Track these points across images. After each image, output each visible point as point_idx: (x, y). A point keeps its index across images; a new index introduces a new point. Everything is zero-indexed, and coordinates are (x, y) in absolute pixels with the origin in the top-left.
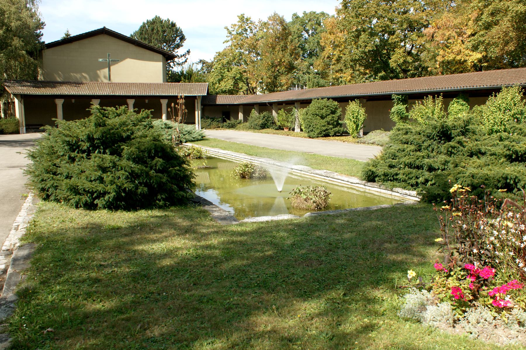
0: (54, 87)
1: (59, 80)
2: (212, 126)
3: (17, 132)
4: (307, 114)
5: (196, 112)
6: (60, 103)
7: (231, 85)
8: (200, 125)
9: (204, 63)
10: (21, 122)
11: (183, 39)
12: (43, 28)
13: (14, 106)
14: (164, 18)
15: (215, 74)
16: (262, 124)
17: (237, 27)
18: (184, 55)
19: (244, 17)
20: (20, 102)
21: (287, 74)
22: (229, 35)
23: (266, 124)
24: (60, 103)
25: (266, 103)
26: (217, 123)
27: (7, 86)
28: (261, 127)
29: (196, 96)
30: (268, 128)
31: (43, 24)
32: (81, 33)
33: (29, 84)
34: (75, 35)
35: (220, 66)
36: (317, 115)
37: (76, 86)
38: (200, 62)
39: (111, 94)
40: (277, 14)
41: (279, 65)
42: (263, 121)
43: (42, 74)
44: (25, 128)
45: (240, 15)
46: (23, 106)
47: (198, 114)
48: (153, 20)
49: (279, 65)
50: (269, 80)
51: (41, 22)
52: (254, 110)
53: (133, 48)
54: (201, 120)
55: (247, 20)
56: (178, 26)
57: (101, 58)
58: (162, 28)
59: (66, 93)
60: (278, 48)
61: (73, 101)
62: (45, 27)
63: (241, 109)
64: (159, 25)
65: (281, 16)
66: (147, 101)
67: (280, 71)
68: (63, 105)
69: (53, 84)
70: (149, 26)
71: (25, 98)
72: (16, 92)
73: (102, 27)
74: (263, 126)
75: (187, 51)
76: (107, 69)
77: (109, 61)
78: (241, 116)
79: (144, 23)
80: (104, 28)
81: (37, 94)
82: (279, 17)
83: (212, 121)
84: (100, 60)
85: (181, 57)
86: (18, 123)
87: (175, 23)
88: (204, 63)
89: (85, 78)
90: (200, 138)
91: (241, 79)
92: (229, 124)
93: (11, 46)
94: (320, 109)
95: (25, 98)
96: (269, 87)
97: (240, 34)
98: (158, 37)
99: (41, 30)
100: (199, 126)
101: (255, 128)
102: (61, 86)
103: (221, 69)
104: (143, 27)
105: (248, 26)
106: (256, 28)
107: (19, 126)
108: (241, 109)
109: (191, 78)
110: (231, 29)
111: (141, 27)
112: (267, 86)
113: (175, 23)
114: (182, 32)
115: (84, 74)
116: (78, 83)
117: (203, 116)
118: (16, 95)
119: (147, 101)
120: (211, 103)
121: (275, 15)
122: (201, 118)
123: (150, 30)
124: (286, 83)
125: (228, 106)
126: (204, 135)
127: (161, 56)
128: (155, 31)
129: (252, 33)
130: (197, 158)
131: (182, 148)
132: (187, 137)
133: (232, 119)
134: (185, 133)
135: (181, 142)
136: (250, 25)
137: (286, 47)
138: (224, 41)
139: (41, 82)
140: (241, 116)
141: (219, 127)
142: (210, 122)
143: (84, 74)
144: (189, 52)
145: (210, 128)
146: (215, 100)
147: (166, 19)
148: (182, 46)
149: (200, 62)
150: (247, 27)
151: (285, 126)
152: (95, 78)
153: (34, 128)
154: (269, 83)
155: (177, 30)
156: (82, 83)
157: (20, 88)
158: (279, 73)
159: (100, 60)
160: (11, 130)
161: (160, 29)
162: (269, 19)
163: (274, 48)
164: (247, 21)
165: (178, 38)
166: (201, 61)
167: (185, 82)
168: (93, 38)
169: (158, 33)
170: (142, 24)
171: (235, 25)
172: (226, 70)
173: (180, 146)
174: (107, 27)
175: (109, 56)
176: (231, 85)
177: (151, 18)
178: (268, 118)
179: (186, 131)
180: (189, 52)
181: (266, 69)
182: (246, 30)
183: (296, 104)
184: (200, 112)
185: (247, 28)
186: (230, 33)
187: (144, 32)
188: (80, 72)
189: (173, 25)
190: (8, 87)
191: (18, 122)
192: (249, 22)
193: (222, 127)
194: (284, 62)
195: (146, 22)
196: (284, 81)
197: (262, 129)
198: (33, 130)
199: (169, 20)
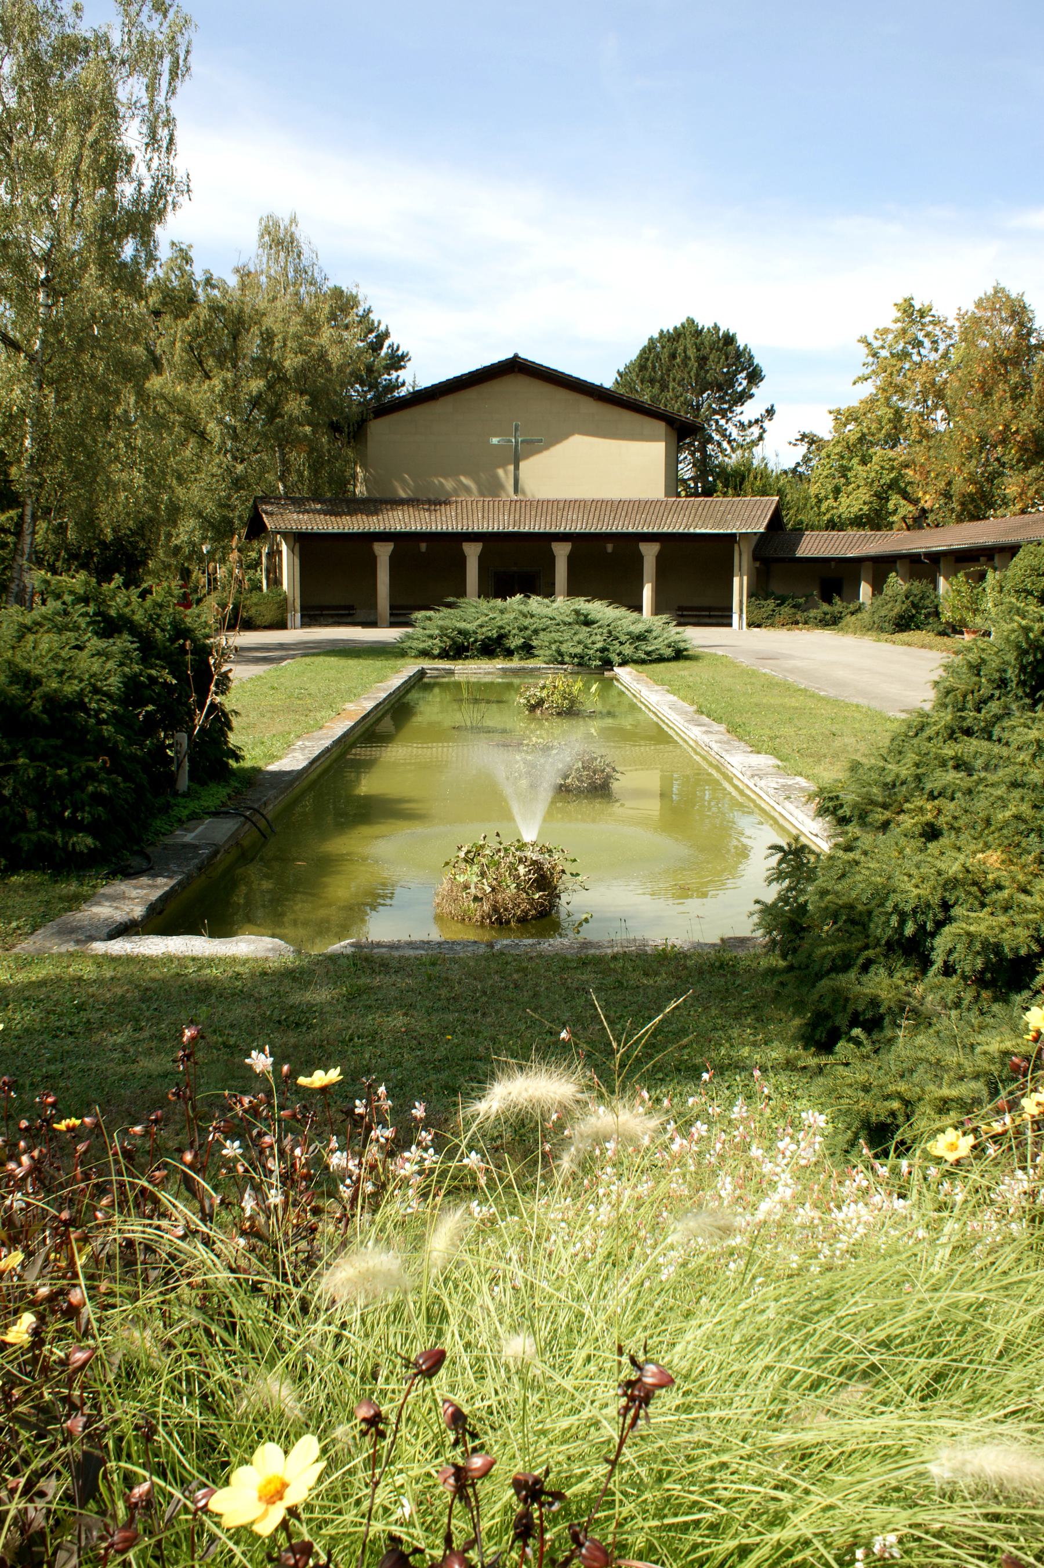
0: (376, 513)
1: (403, 495)
2: (777, 619)
3: (281, 625)
4: (1002, 587)
5: (736, 580)
6: (383, 552)
7: (865, 503)
8: (744, 616)
9: (812, 442)
10: (290, 599)
11: (755, 376)
12: (404, 367)
13: (281, 559)
14: (705, 322)
15: (825, 473)
16: (901, 617)
17: (891, 336)
18: (757, 421)
19: (912, 306)
20: (292, 550)
21: (1026, 469)
22: (870, 359)
23: (913, 616)
24: (383, 552)
25: (918, 555)
26: (793, 610)
27: (266, 513)
28: (897, 625)
29: (733, 535)
30: (918, 628)
31: (403, 357)
32: (458, 374)
33: (319, 506)
34: (429, 385)
35: (838, 449)
36: (1029, 593)
37: (429, 510)
38: (802, 440)
39: (511, 529)
40: (1003, 290)
41: (1004, 441)
42: (904, 607)
43: (366, 480)
44: (298, 615)
45: (900, 301)
46: (297, 561)
47: (740, 585)
48: (675, 328)
49: (1004, 441)
50: (971, 489)
51: (400, 353)
52: (894, 574)
53: (588, 406)
54: (748, 602)
55: (922, 314)
56: (741, 342)
57: (496, 436)
58: (698, 350)
59: (399, 527)
60: (1001, 390)
61: (423, 547)
62: (408, 364)
63: (867, 570)
64: (689, 342)
65: (1014, 296)
66: (610, 548)
67: (1005, 459)
68: (391, 557)
69: (372, 505)
70: (663, 347)
71: (303, 541)
72: (283, 526)
73: (511, 355)
74: (904, 624)
75: (767, 411)
76: (511, 468)
77: (517, 442)
78: (865, 590)
79: (651, 339)
80: (516, 356)
81: (330, 530)
82: (1008, 297)
83: (778, 605)
84: (495, 440)
85: (750, 426)
86: (283, 604)
87: (734, 335)
88: (812, 442)
89: (468, 490)
90: (669, 652)
91: (893, 485)
92: (825, 614)
93: (282, 417)
94: (1038, 575)
95: (303, 541)
96: (971, 507)
97: (905, 355)
98: (686, 376)
99: (400, 372)
100: (741, 617)
101: (882, 630)
102: (392, 509)
103: (842, 457)
104: (648, 354)
105: (923, 333)
106: (949, 336)
107: (286, 610)
108: (867, 570)
109: (741, 484)
110: (877, 344)
111: (644, 351)
112: (962, 504)
113: (734, 335)
114: (751, 357)
115: (463, 479)
116: (436, 502)
117: (758, 592)
118: (285, 535)
119: (610, 548)
120: (781, 555)
121: (996, 292)
122: (749, 596)
123: (665, 357)
124: (1021, 494)
125: (833, 564)
126: (682, 645)
127: (661, 427)
128: (678, 360)
129: (936, 350)
130: (559, 714)
131: (612, 679)
132: (628, 650)
133: (837, 599)
134: (623, 638)
135: (608, 664)
136: (930, 328)
137: (1027, 385)
138: (855, 378)
139: (365, 501)
140: (865, 590)
141: (797, 623)
142: (772, 606)
143: (463, 479)
144: (770, 412)
145: (772, 625)
146: (796, 544)
147: (711, 325)
148: (751, 396)
149: (802, 440)
150: (920, 335)
151: (966, 626)
152: (493, 488)
153: (332, 616)
154: (970, 495)
155: (739, 354)
156: (447, 503)
157: (295, 516)
158: (1003, 465)
159: (495, 440)
160: (269, 617)
161: (692, 353)
162: (979, 304)
163: (988, 394)
164: (922, 317)
165: (744, 375)
166: (804, 436)
167: (725, 494)
168: (469, 390)
169: (686, 365)
170: (646, 343)
171: (886, 331)
172: (855, 461)
173: (607, 674)
174: (522, 355)
175: (516, 429)
176: (865, 503)
177: (671, 322)
178: (922, 598)
179: (629, 634)
180: (770, 412)
181: (962, 456)
182: (920, 344)
183: (942, 560)
184: (745, 578)
185: (921, 338)
186: (875, 355)
187: (649, 364)
188: (453, 474)
189: (729, 340)
190: (270, 514)
191: (286, 599)
192: (928, 319)
193: (806, 623)
194: (1017, 432)
195: (656, 336)
196: (1012, 491)
197: (902, 631)
198: (331, 620)
199: (716, 328)
